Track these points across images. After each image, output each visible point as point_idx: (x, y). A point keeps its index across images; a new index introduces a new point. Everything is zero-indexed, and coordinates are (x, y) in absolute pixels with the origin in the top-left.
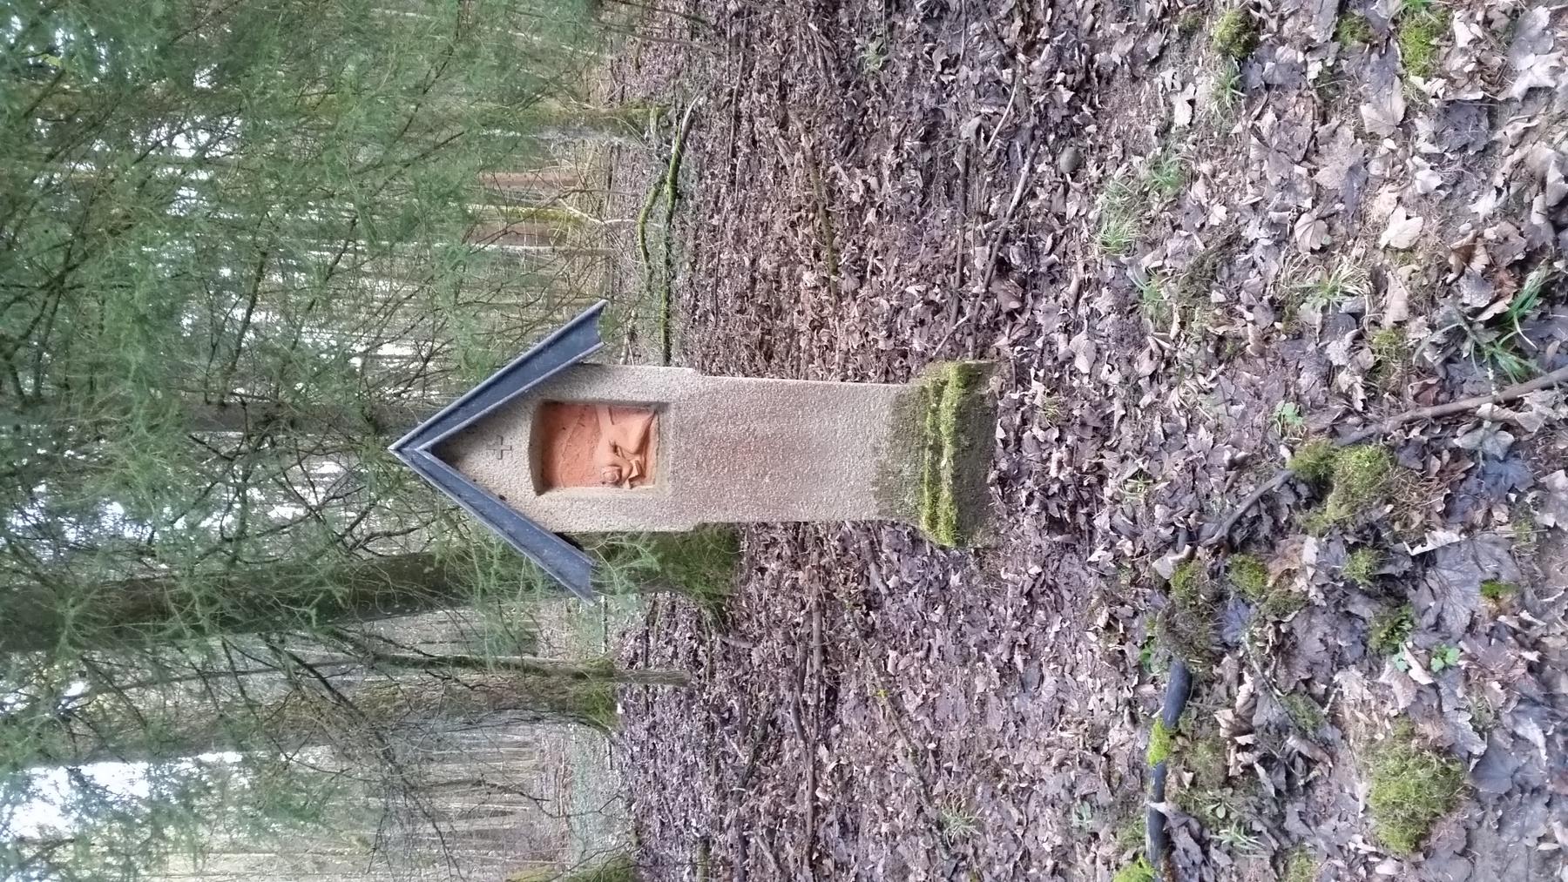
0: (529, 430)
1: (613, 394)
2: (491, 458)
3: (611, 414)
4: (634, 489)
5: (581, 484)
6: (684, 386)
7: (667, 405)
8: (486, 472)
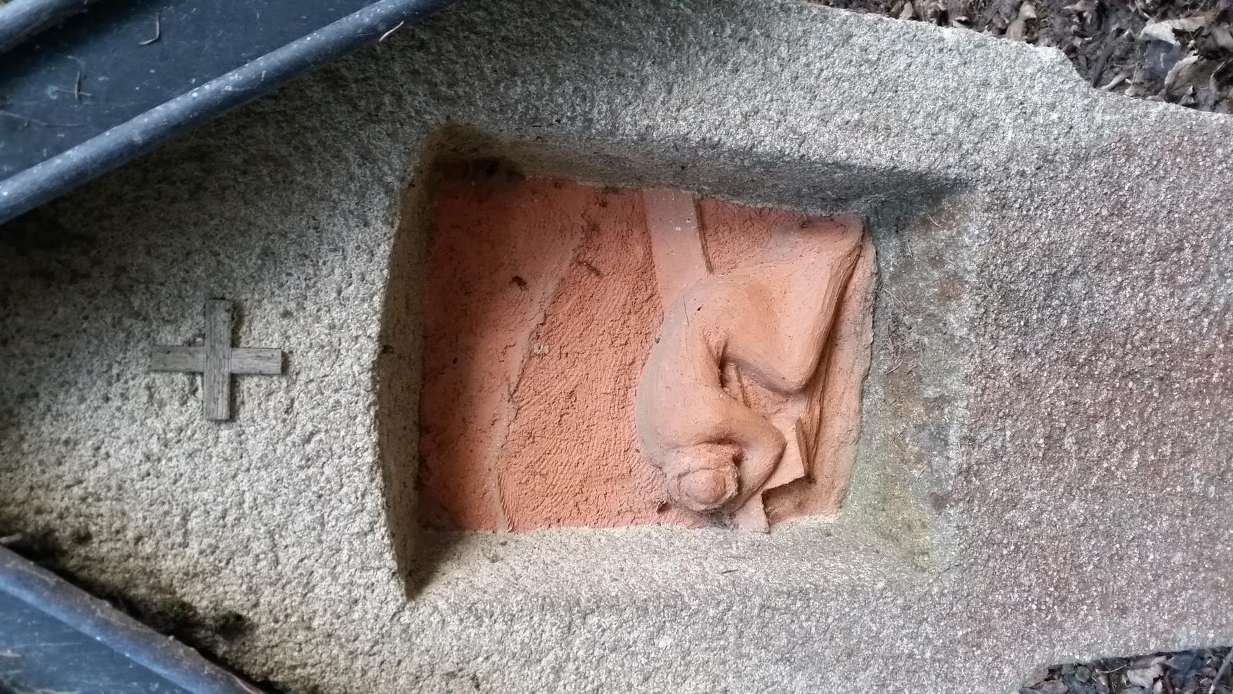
0: (379, 274)
1: (760, 127)
2: (174, 414)
3: (702, 227)
4: (781, 528)
5: (577, 515)
6: (1026, 113)
7: (959, 185)
8: (146, 490)
